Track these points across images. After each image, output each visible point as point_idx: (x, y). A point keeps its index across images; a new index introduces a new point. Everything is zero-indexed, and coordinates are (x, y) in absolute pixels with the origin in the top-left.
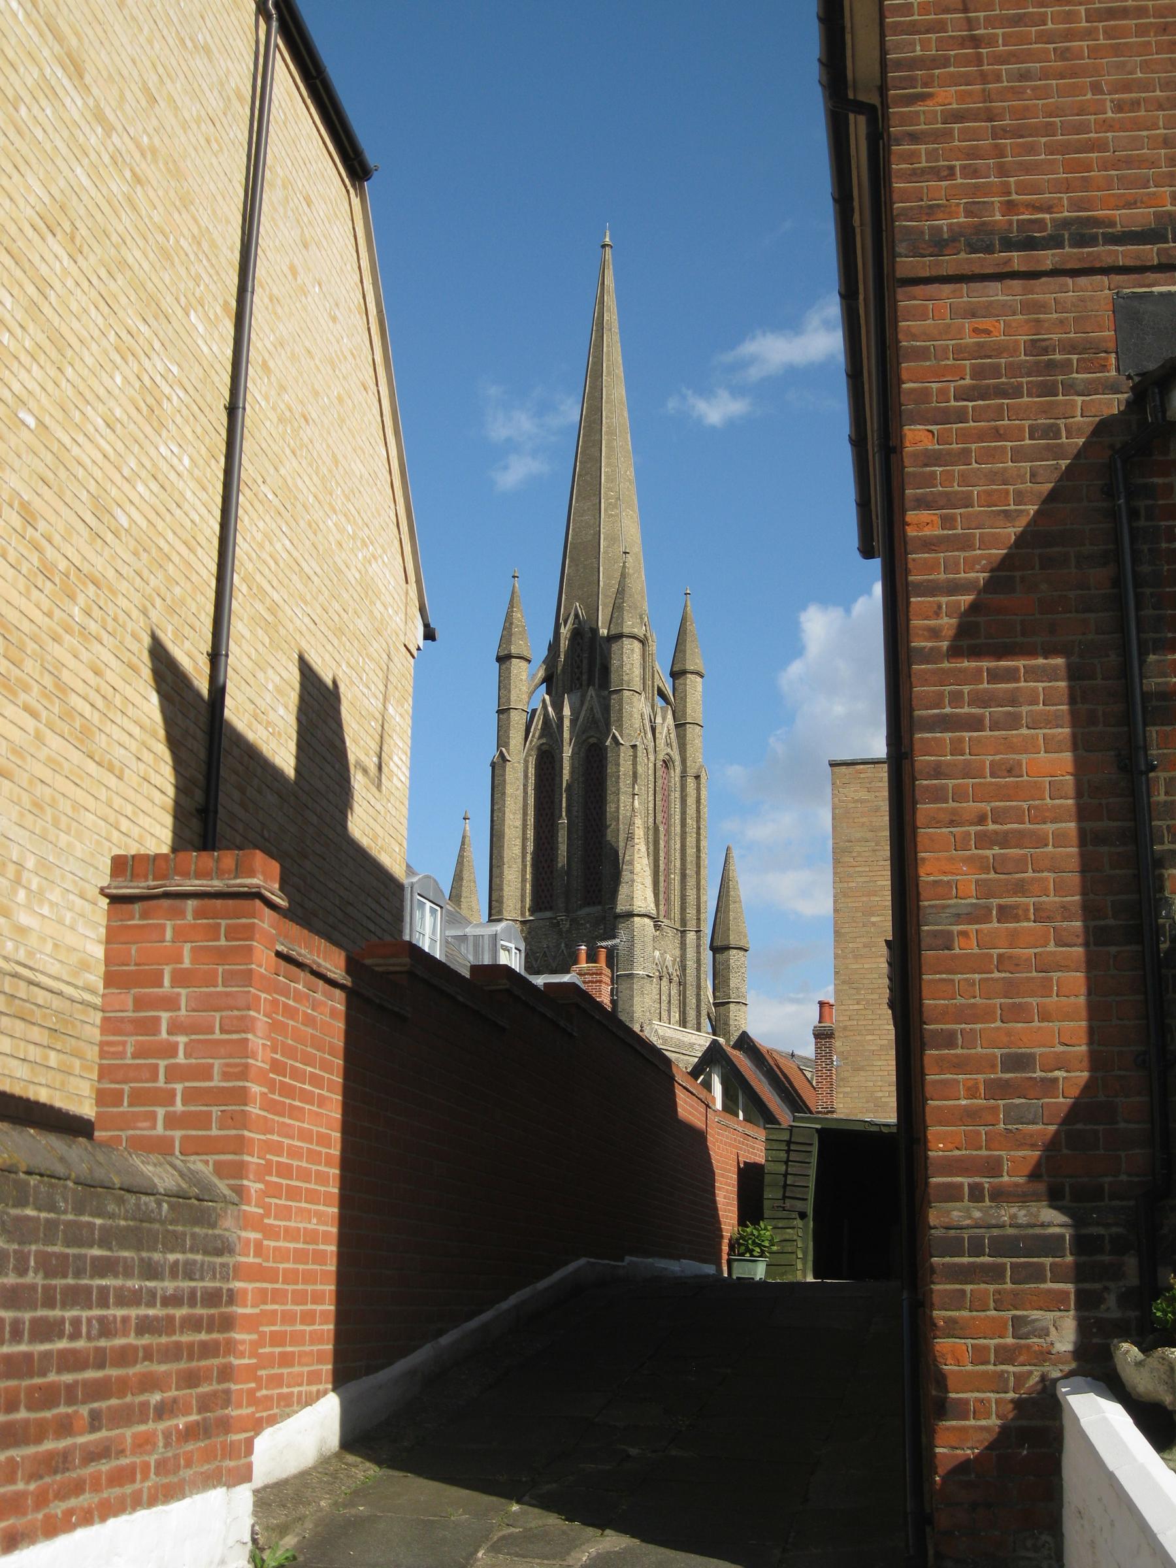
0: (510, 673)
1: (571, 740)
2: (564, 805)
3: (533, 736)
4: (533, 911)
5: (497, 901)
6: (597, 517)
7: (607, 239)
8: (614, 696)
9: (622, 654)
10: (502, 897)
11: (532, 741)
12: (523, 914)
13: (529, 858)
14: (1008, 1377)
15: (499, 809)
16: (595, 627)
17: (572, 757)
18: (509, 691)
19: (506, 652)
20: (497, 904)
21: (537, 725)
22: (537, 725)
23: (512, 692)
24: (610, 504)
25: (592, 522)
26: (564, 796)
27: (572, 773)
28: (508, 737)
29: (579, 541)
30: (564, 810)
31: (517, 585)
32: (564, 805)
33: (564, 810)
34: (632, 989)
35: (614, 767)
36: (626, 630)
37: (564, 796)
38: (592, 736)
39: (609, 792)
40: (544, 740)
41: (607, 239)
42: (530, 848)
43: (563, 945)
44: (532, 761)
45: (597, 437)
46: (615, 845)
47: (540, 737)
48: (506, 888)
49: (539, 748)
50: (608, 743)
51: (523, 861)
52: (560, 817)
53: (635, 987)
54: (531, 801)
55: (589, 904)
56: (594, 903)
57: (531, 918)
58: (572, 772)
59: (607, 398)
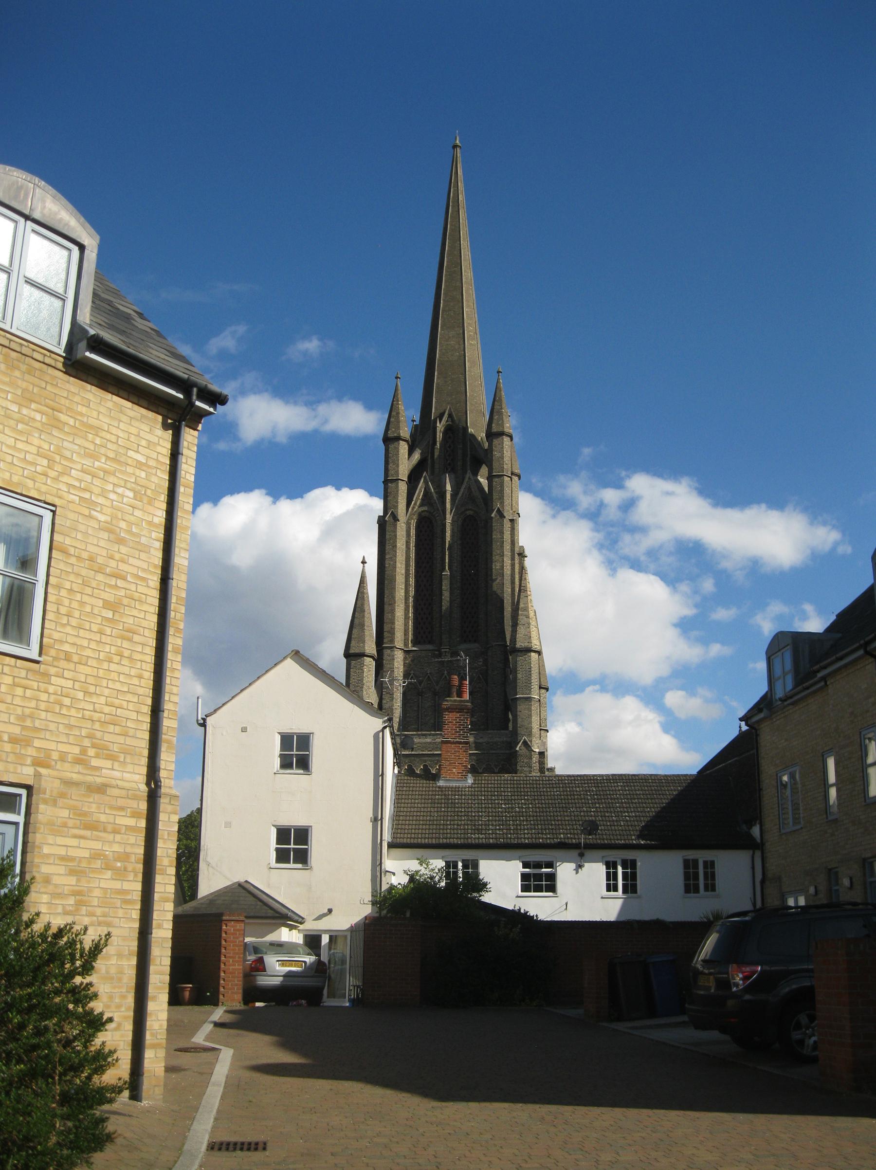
0: (398, 452)
1: (451, 511)
2: (447, 561)
3: (415, 504)
4: (415, 642)
5: (389, 632)
6: (462, 342)
7: (458, 142)
8: (496, 480)
9: (503, 448)
10: (394, 629)
11: (414, 508)
12: (406, 645)
13: (411, 599)
14: (57, 1053)
15: (391, 558)
16: (465, 426)
17: (453, 521)
18: (398, 466)
19: (396, 435)
20: (390, 635)
21: (419, 495)
22: (419, 495)
23: (400, 467)
24: (470, 335)
25: (457, 347)
26: (447, 553)
27: (452, 536)
28: (397, 502)
29: (447, 359)
30: (447, 564)
31: (399, 384)
32: (447, 561)
33: (447, 564)
34: (530, 710)
35: (498, 534)
36: (506, 430)
37: (447, 553)
38: (471, 510)
39: (494, 553)
40: (425, 508)
41: (458, 142)
42: (412, 593)
43: (446, 672)
44: (413, 523)
45: (458, 284)
46: (501, 595)
47: (421, 505)
48: (397, 623)
49: (420, 514)
50: (493, 515)
51: (406, 603)
52: (444, 569)
53: (533, 708)
54: (413, 555)
55: (465, 641)
56: (470, 641)
57: (414, 649)
58: (453, 535)
59: (464, 257)
